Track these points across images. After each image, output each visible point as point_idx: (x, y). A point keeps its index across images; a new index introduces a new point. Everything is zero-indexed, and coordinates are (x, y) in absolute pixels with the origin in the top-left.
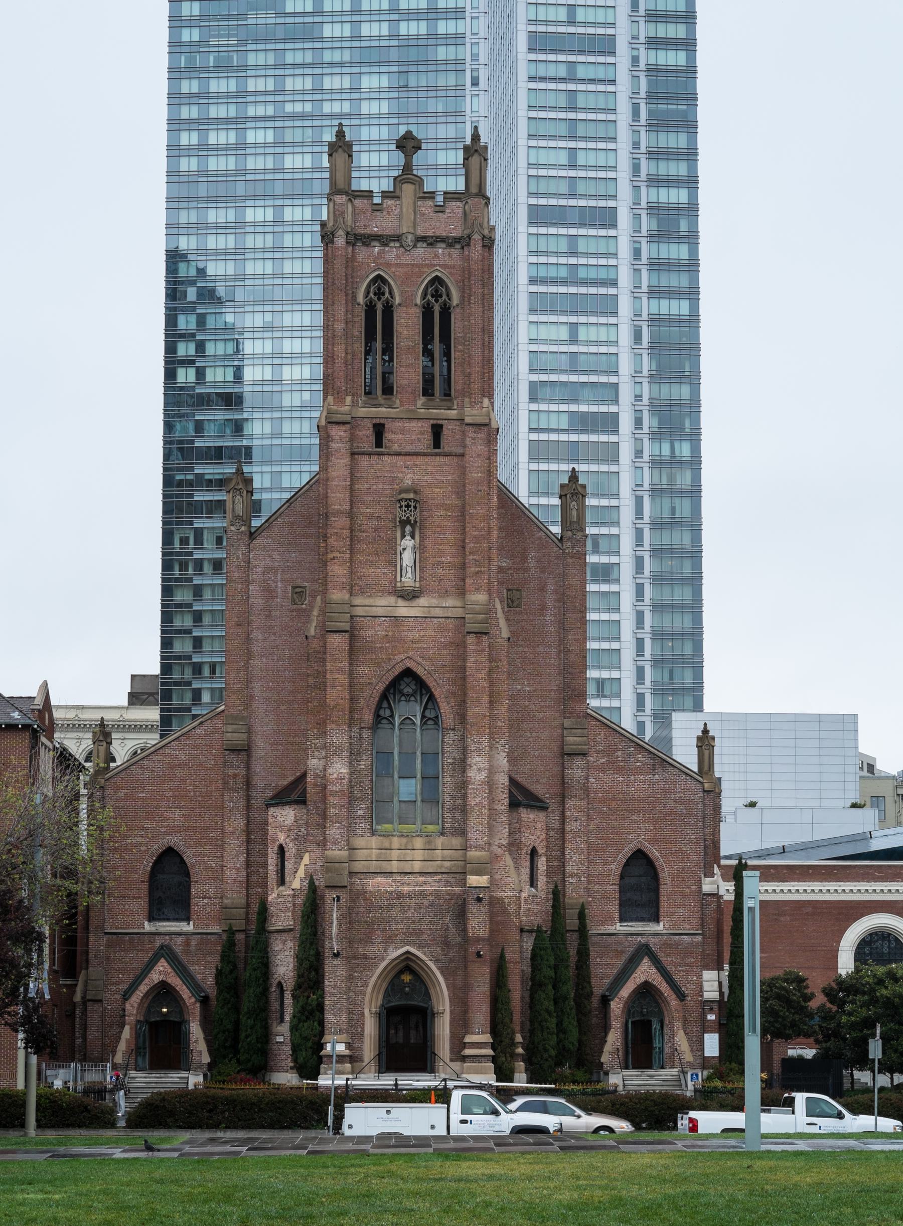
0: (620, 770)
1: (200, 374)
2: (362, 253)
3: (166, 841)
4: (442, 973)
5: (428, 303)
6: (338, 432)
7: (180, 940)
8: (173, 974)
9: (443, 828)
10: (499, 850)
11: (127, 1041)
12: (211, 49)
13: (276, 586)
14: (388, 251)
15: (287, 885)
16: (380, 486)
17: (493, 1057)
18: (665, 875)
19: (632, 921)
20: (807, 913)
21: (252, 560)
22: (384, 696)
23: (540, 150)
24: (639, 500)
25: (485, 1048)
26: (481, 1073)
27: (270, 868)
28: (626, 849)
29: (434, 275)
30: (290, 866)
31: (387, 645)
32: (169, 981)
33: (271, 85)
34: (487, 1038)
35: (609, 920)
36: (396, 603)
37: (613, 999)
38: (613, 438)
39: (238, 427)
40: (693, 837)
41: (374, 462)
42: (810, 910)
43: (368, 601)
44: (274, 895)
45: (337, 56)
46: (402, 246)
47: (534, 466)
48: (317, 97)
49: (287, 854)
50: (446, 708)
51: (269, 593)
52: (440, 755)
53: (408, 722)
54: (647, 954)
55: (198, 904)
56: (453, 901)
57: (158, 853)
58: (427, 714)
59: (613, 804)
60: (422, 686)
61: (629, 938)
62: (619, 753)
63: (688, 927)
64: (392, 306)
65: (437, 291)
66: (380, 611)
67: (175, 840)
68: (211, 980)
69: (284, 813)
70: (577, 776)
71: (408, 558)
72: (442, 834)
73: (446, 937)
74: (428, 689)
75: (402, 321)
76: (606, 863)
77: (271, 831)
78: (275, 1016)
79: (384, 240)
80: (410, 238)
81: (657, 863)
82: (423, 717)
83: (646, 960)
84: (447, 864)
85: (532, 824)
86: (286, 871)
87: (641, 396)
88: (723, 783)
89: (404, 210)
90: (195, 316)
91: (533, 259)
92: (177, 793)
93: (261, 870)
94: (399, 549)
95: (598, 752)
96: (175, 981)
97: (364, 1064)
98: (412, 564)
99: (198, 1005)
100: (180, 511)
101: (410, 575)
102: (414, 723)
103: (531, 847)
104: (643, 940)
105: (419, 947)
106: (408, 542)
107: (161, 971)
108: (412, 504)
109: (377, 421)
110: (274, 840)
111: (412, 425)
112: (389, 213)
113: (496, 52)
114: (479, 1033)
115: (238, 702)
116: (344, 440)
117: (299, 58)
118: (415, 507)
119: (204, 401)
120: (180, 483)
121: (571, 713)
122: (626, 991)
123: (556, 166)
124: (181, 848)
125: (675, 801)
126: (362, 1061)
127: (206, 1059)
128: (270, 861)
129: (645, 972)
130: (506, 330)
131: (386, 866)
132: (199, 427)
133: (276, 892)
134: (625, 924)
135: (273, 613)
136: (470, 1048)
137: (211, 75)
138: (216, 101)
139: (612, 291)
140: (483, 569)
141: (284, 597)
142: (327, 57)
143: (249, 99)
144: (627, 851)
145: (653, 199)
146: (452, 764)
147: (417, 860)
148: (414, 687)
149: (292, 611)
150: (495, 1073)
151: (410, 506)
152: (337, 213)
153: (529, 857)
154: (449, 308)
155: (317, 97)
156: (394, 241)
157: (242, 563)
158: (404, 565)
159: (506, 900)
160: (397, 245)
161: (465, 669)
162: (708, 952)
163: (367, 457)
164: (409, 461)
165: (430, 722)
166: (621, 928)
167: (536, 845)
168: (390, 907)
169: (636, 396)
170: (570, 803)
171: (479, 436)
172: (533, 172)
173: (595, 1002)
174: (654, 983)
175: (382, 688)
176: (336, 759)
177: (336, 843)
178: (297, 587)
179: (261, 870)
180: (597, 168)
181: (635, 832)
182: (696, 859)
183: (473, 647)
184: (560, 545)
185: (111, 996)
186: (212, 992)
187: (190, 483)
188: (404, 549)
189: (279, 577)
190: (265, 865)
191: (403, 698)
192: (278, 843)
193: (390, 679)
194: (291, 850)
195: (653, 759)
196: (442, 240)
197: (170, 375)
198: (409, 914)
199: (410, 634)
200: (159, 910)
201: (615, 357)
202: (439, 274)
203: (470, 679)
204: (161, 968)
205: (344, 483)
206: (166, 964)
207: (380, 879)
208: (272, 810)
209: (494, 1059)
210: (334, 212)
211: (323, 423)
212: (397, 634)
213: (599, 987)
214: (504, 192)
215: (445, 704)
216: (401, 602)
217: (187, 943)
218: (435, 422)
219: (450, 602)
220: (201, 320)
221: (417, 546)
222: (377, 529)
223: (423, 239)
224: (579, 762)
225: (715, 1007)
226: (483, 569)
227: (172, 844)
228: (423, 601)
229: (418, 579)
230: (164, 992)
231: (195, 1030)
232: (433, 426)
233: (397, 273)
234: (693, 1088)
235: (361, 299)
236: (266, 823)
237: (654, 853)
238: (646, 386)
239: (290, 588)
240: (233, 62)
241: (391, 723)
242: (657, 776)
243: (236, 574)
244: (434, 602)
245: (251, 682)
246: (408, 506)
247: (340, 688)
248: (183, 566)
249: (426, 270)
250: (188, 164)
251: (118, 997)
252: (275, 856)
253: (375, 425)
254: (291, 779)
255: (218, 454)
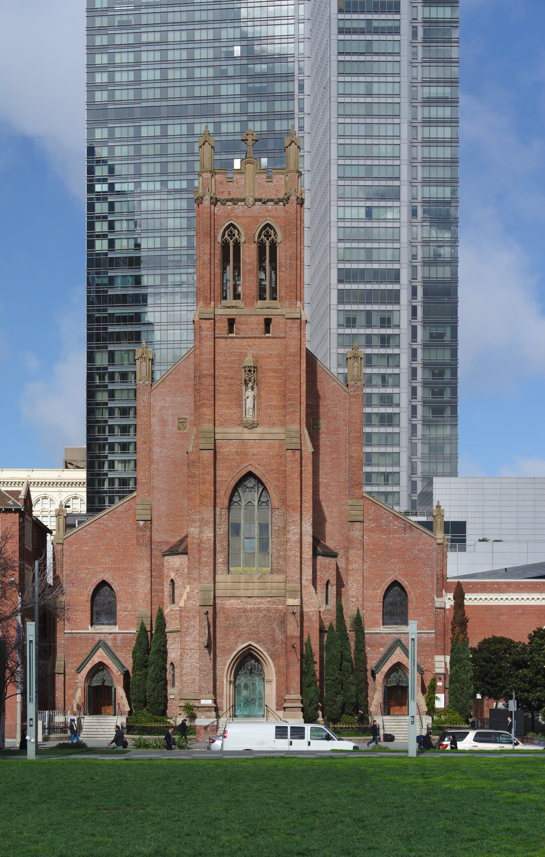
0: (383, 531)
1: (111, 243)
2: (219, 209)
3: (101, 576)
4: (271, 657)
5: (262, 241)
6: (207, 325)
7: (111, 637)
8: (107, 657)
9: (272, 569)
10: (306, 582)
11: (80, 698)
12: (116, 13)
13: (168, 419)
14: (237, 208)
15: (176, 604)
16: (233, 358)
17: (302, 708)
18: (411, 596)
19: (390, 624)
20: (519, 613)
21: (152, 402)
22: (235, 489)
23: (347, 84)
24: (414, 329)
25: (297, 703)
26: (295, 718)
27: (166, 593)
28: (387, 580)
29: (266, 223)
30: (178, 592)
31: (237, 457)
32: (105, 662)
33: (158, 37)
34: (299, 697)
35: (375, 624)
36: (243, 431)
37: (377, 673)
38: (396, 287)
39: (138, 280)
40: (430, 572)
41: (228, 343)
42: (520, 611)
43: (225, 430)
44: (168, 610)
45: (204, 16)
46: (245, 204)
47: (341, 307)
48: (190, 83)
49: (176, 585)
50: (274, 496)
51: (164, 423)
52: (270, 524)
53: (250, 504)
54: (399, 646)
55: (120, 614)
56: (278, 614)
57: (97, 584)
58: (263, 499)
59: (380, 552)
60: (259, 481)
61: (389, 635)
62: (383, 521)
63: (425, 628)
64: (239, 243)
65: (267, 232)
66: (232, 436)
67: (107, 577)
68: (131, 661)
69: (174, 560)
70: (356, 535)
71: (249, 403)
72: (272, 573)
73: (274, 636)
74: (263, 484)
75: (246, 253)
76: (374, 589)
77: (166, 571)
78: (169, 683)
79: (235, 201)
80: (251, 200)
81: (406, 589)
82: (259, 501)
83: (398, 649)
84: (274, 591)
85: (327, 566)
86: (176, 595)
87: (416, 256)
88: (467, 525)
89: (247, 181)
90: (107, 203)
91: (341, 162)
92: (108, 547)
93: (160, 594)
94: (244, 397)
95: (370, 520)
96: (108, 662)
97: (224, 712)
98: (252, 406)
99: (122, 676)
100: (98, 340)
101: (251, 413)
102: (254, 505)
103: (327, 580)
104: (397, 636)
105: (258, 642)
106: (250, 393)
107: (100, 656)
108: (252, 369)
109: (231, 317)
110: (168, 577)
111: (253, 319)
112: (237, 183)
113: (316, 11)
114: (293, 694)
115: (145, 491)
116: (210, 330)
117: (177, 18)
118: (254, 371)
119: (114, 263)
120: (98, 320)
121: (353, 495)
122: (385, 668)
123: (358, 95)
124: (110, 581)
125: (418, 550)
126: (222, 710)
127: (127, 709)
128: (165, 589)
129: (397, 656)
130: (322, 211)
131: (238, 593)
132: (112, 280)
133: (170, 608)
134: (386, 626)
135: (166, 435)
136: (288, 702)
137: (116, 32)
138: (126, 87)
139: (396, 183)
140: (297, 410)
141: (173, 425)
142: (197, 16)
143: (143, 30)
144: (388, 581)
145: (426, 115)
146: (278, 530)
147: (255, 589)
148: (254, 483)
149: (178, 434)
150: (304, 718)
151: (251, 371)
152: (204, 184)
153: (325, 586)
154: (276, 244)
155: (190, 83)
156: (241, 201)
157: (147, 404)
158: (247, 407)
159: (311, 613)
160: (243, 203)
161: (285, 471)
162: (438, 644)
163: (224, 340)
164: (251, 342)
165: (264, 504)
166: (384, 629)
167: (330, 579)
168: (239, 617)
169: (413, 256)
170: (352, 552)
171: (294, 325)
172: (341, 100)
173: (369, 674)
174: (404, 663)
175: (234, 484)
176: (206, 528)
177: (206, 579)
178: (181, 419)
179: (160, 594)
180: (386, 95)
181: (393, 570)
182: (431, 586)
183: (290, 459)
184: (346, 389)
185: (70, 670)
186: (130, 668)
187: (105, 319)
188: (248, 397)
189: (170, 412)
190: (162, 591)
191: (247, 490)
192: (170, 578)
193: (239, 478)
194: (178, 583)
195: (405, 524)
196: (271, 200)
197: (91, 245)
198: (251, 622)
199: (251, 450)
200: (97, 618)
201: (398, 229)
202: (269, 222)
203: (288, 478)
204: (100, 654)
205: (210, 357)
206: (102, 652)
207: (233, 601)
208: (166, 558)
209: (303, 710)
210: (203, 184)
211: (197, 319)
212: (243, 450)
213: (371, 664)
214: (321, 114)
215: (273, 493)
216: (246, 430)
217: (115, 639)
218: (266, 317)
219: (276, 430)
220: (112, 206)
221: (256, 395)
222: (230, 385)
223: (260, 200)
224: (358, 526)
225: (442, 677)
226: (297, 410)
227: (105, 579)
228: (259, 430)
229: (256, 416)
230: (100, 667)
231: (120, 692)
232: (266, 319)
233: (242, 222)
234: (426, 727)
235: (219, 239)
236: (163, 565)
237: (405, 583)
238: (420, 249)
239: (176, 419)
240: (131, 23)
241: (240, 505)
242: (407, 535)
243: (143, 411)
244: (266, 430)
245: (153, 478)
246: (250, 371)
247: (208, 484)
248: (102, 378)
249: (260, 219)
250: (101, 96)
251: (73, 671)
252: (168, 586)
253: (229, 320)
254: (178, 539)
255: (122, 300)
